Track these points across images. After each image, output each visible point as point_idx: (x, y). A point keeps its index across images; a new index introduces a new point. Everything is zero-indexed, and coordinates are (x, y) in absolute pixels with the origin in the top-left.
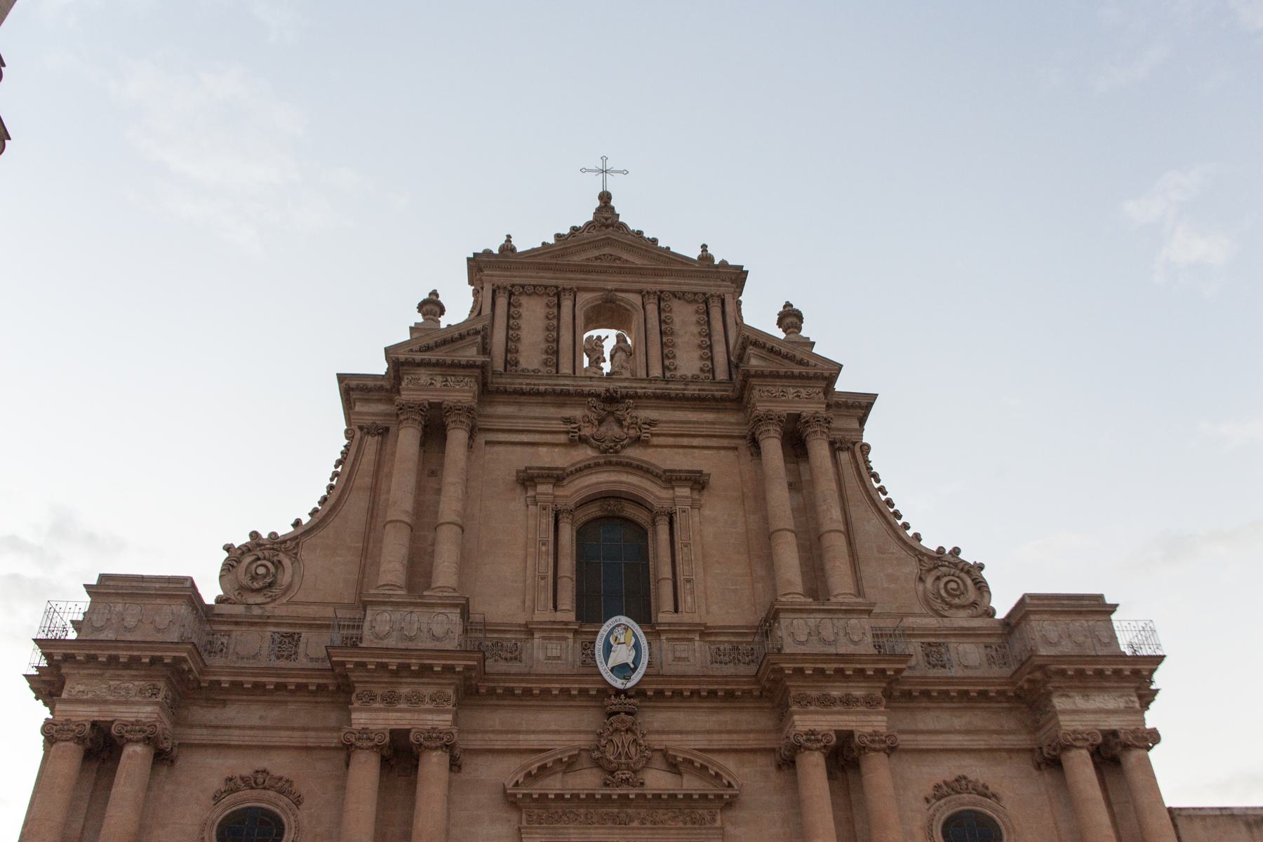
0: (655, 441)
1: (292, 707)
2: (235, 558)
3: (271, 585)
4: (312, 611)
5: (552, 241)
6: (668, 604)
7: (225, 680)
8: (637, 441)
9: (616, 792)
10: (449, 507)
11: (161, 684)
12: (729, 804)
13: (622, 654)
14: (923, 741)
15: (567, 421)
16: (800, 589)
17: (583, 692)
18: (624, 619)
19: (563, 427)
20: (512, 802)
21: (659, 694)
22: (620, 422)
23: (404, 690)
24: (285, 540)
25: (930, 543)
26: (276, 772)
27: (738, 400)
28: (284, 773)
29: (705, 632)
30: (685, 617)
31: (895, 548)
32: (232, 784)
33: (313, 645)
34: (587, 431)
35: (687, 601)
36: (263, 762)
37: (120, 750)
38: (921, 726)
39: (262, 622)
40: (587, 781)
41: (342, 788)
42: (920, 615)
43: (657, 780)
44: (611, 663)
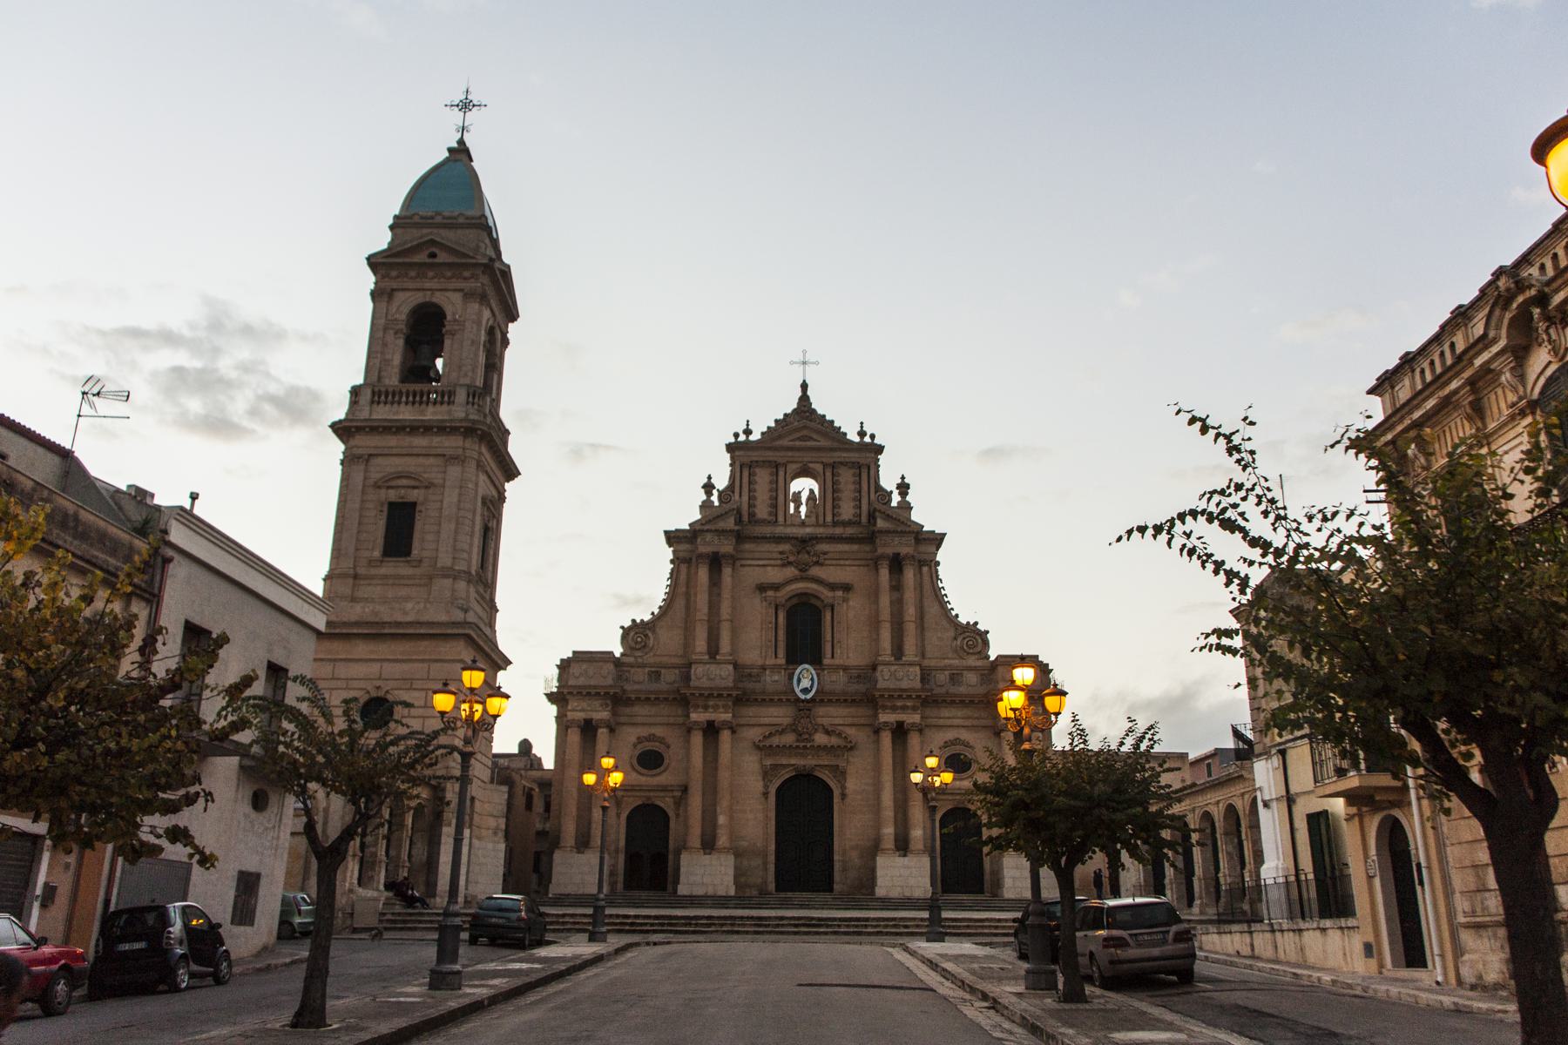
0: (827, 562)
1: (662, 706)
2: (626, 632)
3: (644, 646)
4: (665, 660)
5: (773, 425)
6: (829, 654)
7: (633, 696)
8: (817, 563)
9: (802, 745)
10: (725, 610)
11: (609, 702)
12: (851, 749)
13: (806, 683)
14: (941, 722)
15: (781, 553)
16: (889, 652)
17: (788, 700)
18: (807, 666)
19: (780, 556)
20: (758, 748)
21: (822, 701)
22: (808, 553)
23: (711, 703)
24: (648, 623)
25: (963, 620)
26: (658, 734)
27: (870, 538)
28: (662, 735)
29: (845, 669)
30: (837, 661)
31: (944, 622)
32: (640, 740)
33: (670, 676)
34: (792, 559)
35: (838, 651)
36: (653, 730)
37: (596, 730)
38: (942, 715)
39: (643, 666)
40: (789, 739)
41: (688, 741)
42: (953, 659)
43: (820, 739)
44: (801, 687)
